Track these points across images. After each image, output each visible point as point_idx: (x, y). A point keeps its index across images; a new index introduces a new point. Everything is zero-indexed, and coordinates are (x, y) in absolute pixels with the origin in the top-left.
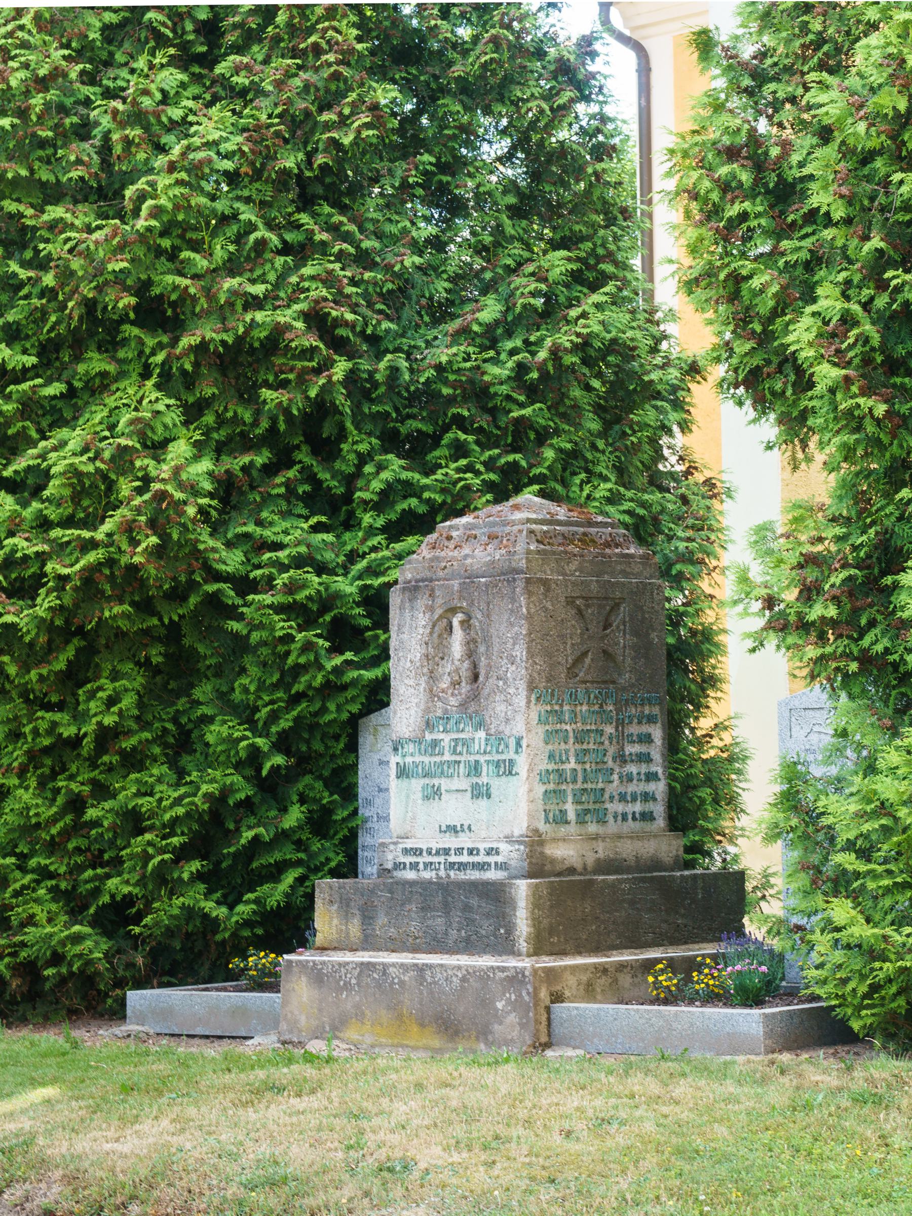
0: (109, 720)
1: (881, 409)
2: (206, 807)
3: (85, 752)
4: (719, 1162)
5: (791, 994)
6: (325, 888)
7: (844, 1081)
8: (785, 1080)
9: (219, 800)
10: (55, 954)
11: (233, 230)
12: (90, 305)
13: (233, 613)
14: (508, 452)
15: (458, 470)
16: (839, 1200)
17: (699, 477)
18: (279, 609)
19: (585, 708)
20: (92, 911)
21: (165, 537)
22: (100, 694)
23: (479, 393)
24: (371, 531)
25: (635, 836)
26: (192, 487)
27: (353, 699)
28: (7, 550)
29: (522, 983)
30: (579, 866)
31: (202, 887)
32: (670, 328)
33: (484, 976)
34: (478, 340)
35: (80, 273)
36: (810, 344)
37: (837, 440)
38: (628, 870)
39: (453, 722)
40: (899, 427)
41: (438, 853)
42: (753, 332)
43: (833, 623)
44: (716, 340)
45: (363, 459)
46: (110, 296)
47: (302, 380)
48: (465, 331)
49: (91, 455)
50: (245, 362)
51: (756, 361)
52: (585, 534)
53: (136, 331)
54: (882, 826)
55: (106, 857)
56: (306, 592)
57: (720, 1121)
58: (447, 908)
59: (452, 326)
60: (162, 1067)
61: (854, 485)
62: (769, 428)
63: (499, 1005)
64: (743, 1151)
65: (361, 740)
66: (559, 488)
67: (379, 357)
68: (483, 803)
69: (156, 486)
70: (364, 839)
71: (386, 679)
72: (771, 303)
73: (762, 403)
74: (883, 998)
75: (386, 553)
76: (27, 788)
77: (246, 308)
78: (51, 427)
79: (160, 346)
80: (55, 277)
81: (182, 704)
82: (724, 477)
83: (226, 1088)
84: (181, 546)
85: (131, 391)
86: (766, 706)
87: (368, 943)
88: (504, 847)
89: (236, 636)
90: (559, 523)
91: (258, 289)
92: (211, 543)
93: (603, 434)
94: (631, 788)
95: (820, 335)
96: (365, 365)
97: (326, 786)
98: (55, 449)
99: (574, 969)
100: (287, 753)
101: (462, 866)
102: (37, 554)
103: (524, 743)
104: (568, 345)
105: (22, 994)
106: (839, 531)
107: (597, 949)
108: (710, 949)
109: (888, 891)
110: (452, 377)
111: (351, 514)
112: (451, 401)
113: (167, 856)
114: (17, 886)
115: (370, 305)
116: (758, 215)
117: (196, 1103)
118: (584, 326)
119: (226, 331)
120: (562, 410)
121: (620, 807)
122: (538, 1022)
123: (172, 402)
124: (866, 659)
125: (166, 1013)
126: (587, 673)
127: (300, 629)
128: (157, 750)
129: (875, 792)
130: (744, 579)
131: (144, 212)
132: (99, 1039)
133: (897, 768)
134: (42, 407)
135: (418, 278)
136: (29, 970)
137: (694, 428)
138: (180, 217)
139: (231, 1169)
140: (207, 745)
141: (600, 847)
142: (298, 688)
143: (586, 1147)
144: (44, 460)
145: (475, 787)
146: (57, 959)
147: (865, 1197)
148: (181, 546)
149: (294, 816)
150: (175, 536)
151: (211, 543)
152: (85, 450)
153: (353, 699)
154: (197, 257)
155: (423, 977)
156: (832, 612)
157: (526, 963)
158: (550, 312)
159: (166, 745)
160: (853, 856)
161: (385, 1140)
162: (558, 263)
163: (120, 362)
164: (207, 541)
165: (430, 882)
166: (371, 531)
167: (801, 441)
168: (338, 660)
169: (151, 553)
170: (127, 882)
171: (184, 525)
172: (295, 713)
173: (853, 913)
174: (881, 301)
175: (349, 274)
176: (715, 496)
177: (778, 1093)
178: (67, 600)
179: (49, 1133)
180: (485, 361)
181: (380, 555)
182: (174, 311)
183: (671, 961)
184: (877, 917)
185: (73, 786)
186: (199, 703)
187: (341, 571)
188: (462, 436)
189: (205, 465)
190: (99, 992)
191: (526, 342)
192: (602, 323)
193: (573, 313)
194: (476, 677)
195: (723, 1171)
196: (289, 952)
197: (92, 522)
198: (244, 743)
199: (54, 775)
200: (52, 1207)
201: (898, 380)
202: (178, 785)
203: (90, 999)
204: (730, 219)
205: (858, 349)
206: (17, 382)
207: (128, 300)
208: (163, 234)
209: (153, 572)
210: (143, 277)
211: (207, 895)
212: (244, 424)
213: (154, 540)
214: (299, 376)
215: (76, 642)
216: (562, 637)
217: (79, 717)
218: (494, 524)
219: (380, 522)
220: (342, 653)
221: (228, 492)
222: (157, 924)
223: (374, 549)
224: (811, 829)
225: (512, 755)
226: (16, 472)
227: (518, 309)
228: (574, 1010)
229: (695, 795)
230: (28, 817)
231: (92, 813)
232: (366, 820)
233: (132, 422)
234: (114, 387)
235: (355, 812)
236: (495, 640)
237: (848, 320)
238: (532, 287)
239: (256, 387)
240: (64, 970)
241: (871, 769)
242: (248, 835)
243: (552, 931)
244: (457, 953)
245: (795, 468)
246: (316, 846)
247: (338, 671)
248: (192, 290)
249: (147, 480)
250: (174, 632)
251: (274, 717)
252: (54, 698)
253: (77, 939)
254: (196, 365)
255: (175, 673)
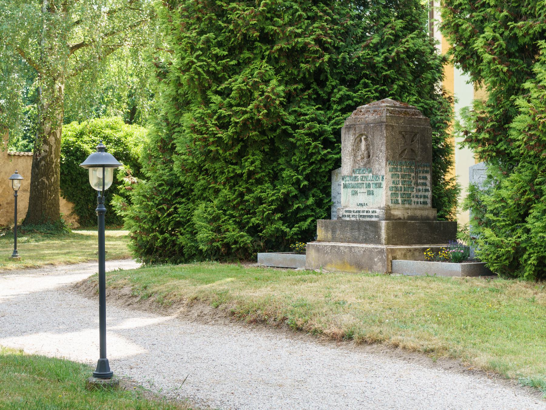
0: (252, 168)
1: (505, 69)
2: (282, 197)
3: (244, 179)
4: (445, 306)
5: (472, 260)
6: (320, 223)
7: (487, 285)
8: (468, 284)
9: (287, 195)
10: (235, 241)
11: (291, 11)
12: (245, 35)
13: (291, 135)
14: (382, 86)
15: (366, 92)
16: (483, 319)
17: (447, 96)
18: (306, 134)
19: (405, 167)
20: (247, 228)
21: (269, 110)
22: (249, 160)
23: (372, 66)
24: (336, 111)
25: (420, 209)
26: (278, 95)
27: (330, 164)
28: (219, 113)
29: (383, 253)
30: (402, 218)
31: (281, 222)
32: (436, 46)
33: (371, 251)
34: (372, 49)
35: (241, 25)
36: (482, 47)
37: (490, 79)
38: (418, 220)
39: (361, 170)
40: (511, 75)
41: (356, 212)
42: (463, 43)
43: (488, 140)
44: (450, 46)
45: (334, 87)
46: (251, 33)
47: (314, 61)
48: (367, 46)
49: (245, 83)
50: (294, 55)
51: (463, 53)
52: (405, 111)
53: (259, 44)
54: (502, 206)
55: (251, 211)
56: (315, 130)
57: (446, 295)
58: (359, 229)
59: (363, 44)
60: (269, 274)
61: (496, 95)
62: (468, 76)
63: (376, 260)
64: (452, 303)
65: (332, 178)
66: (399, 98)
67: (339, 53)
68: (371, 196)
69: (266, 94)
70: (333, 209)
71: (340, 158)
72: (469, 34)
73: (466, 68)
74: (501, 260)
75: (341, 118)
76: (226, 189)
77: (295, 37)
78: (232, 75)
79: (267, 49)
80: (233, 26)
81: (275, 164)
82: (455, 96)
83: (288, 280)
84: (274, 114)
85: (258, 63)
86: (466, 168)
87: (334, 239)
88: (378, 210)
89: (292, 143)
90: (397, 107)
91: (299, 31)
92: (284, 113)
93: (413, 81)
94: (420, 194)
95: (485, 44)
96: (334, 57)
97: (321, 192)
98: (234, 81)
99: (400, 249)
100: (309, 181)
101: (364, 216)
102: (228, 115)
103: (385, 178)
104: (402, 51)
105: (225, 254)
106: (490, 109)
107: (407, 244)
108: (445, 246)
109: (504, 226)
110: (363, 61)
111: (330, 105)
112: (363, 69)
113: (270, 212)
114: (223, 219)
115: (336, 37)
116: (465, 4)
117: (279, 284)
118: (408, 45)
119: (289, 44)
120: (400, 72)
121: (416, 200)
122: (388, 265)
123: (271, 67)
124: (498, 152)
125: (270, 260)
126: (405, 156)
127: (313, 141)
128: (267, 179)
129: (500, 195)
130: (458, 125)
131: (262, 5)
132: (249, 267)
133: (507, 187)
134: (230, 68)
135: (352, 28)
136: (227, 246)
137: (445, 79)
138: (273, 7)
139: (289, 301)
140: (283, 178)
141: (409, 212)
142: (311, 160)
143: (402, 300)
144: (230, 85)
145: (368, 191)
146: (236, 242)
147: (492, 318)
148: (274, 114)
149: (311, 201)
150: (272, 110)
151: (284, 113)
152: (243, 82)
153: (330, 164)
154: (279, 20)
155: (351, 250)
156: (487, 136)
157: (384, 247)
158: (397, 38)
159: (270, 177)
160: (492, 215)
161: (337, 295)
162: (399, 24)
163: (255, 54)
164: (282, 112)
165: (354, 221)
166: (336, 111)
167: (479, 81)
168: (325, 152)
169: (264, 116)
170: (258, 219)
171: (275, 107)
172: (311, 168)
173: (491, 233)
174: (507, 33)
175: (329, 26)
176: (451, 102)
177: (465, 287)
178: (238, 130)
179: (233, 290)
180: (374, 56)
181: (339, 118)
182: (272, 38)
183: (432, 249)
184: (500, 235)
185: (240, 189)
186: (280, 164)
187: (326, 123)
188: (367, 81)
189: (282, 88)
190: (249, 253)
191: (388, 50)
192: (413, 44)
193: (404, 40)
194: (369, 156)
195: (446, 309)
196: (309, 241)
197: (246, 105)
198: (295, 177)
199: (234, 185)
200: (234, 310)
201: (512, 60)
202: (273, 190)
203: (247, 255)
204: (456, 6)
205: (498, 49)
206: (222, 60)
207: (257, 34)
208: (268, 12)
209: (265, 121)
210: (262, 26)
211: (283, 225)
212: (295, 75)
213: (265, 111)
214: (313, 60)
215: (241, 143)
216: (397, 144)
217: (242, 167)
218: (376, 107)
219: (339, 108)
220: (327, 149)
221: (290, 97)
222: (267, 233)
223: (337, 116)
224: (478, 207)
225: (380, 181)
226: (221, 89)
227: (385, 39)
228: (399, 263)
229: (442, 199)
230: (226, 198)
231: (246, 198)
232: (334, 203)
233: (258, 73)
234: (252, 62)
235: (330, 200)
236: (376, 145)
237: (495, 39)
238: (390, 31)
239: (299, 63)
240: (238, 246)
241: (499, 188)
242: (297, 206)
243: (393, 237)
244: (362, 243)
245: (477, 90)
246: (318, 210)
247: (325, 155)
248: (278, 31)
249: (263, 92)
250: (272, 141)
251: (304, 169)
252: (234, 161)
253: (242, 236)
254: (279, 55)
255: (272, 155)
